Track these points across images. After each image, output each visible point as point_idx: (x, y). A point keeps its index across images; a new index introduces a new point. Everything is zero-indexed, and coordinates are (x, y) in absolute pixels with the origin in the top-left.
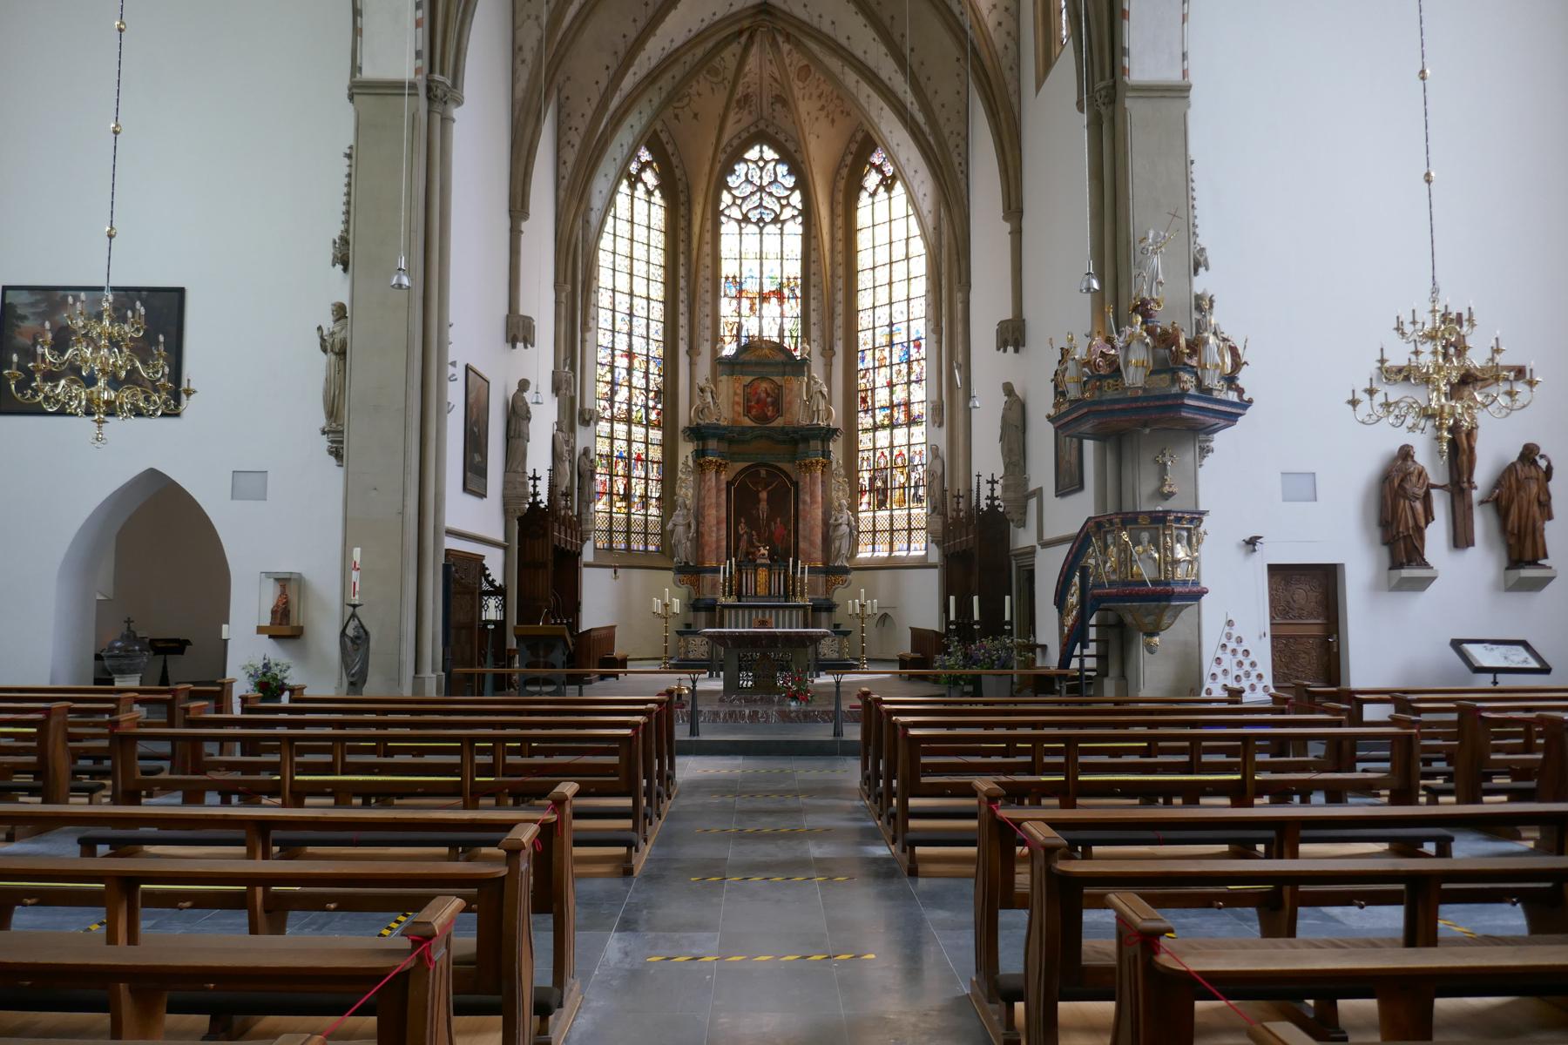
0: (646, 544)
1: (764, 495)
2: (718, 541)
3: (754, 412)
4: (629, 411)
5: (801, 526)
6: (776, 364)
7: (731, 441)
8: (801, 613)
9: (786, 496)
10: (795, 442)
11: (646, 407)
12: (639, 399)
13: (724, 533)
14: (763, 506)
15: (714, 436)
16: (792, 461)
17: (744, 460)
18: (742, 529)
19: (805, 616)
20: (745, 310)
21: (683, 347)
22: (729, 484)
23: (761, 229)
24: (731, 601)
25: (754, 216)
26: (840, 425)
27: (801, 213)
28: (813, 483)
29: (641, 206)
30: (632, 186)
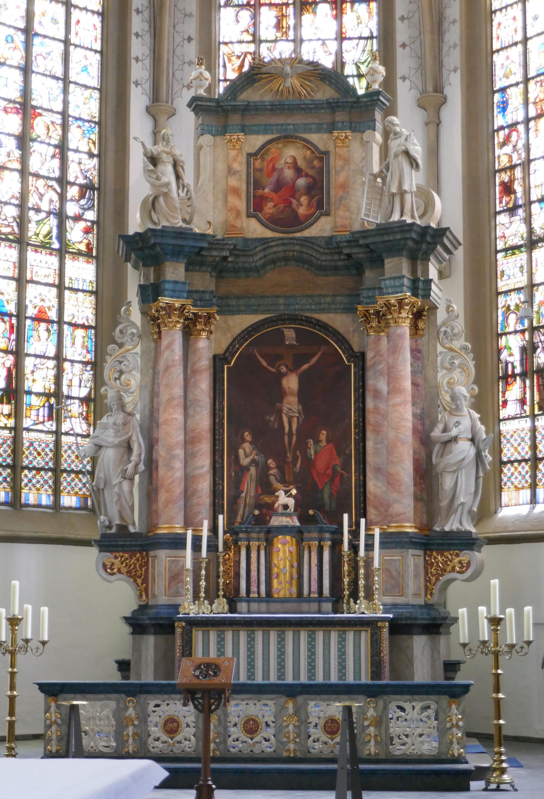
0: (57, 493)
1: (291, 383)
2: (189, 479)
3: (269, 208)
4: (22, 221)
5: (370, 444)
6: (314, 107)
7: (221, 270)
8: (365, 637)
9: (339, 386)
10: (358, 269)
11: (61, 216)
12: (45, 197)
13: (204, 462)
14: (291, 405)
15: (176, 253)
16: (350, 310)
17: (250, 310)
18: (247, 454)
19: (375, 643)
20: (267, 31)
21: (138, 100)
22: (218, 361)
24: (219, 609)
26: (457, 225)
28: (395, 350)
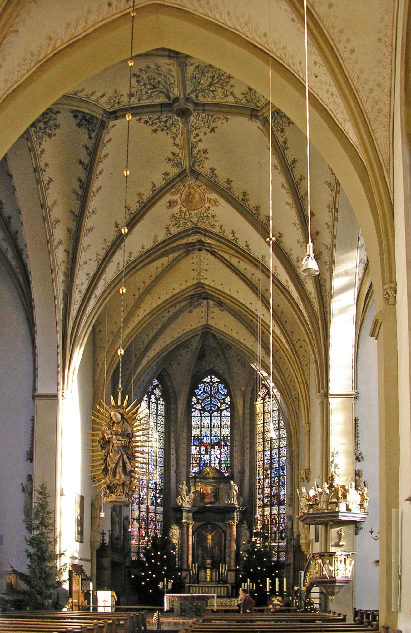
1: (210, 537)
23: (211, 414)
25: (208, 408)
27: (230, 406)
29: (153, 406)
30: (149, 397)
